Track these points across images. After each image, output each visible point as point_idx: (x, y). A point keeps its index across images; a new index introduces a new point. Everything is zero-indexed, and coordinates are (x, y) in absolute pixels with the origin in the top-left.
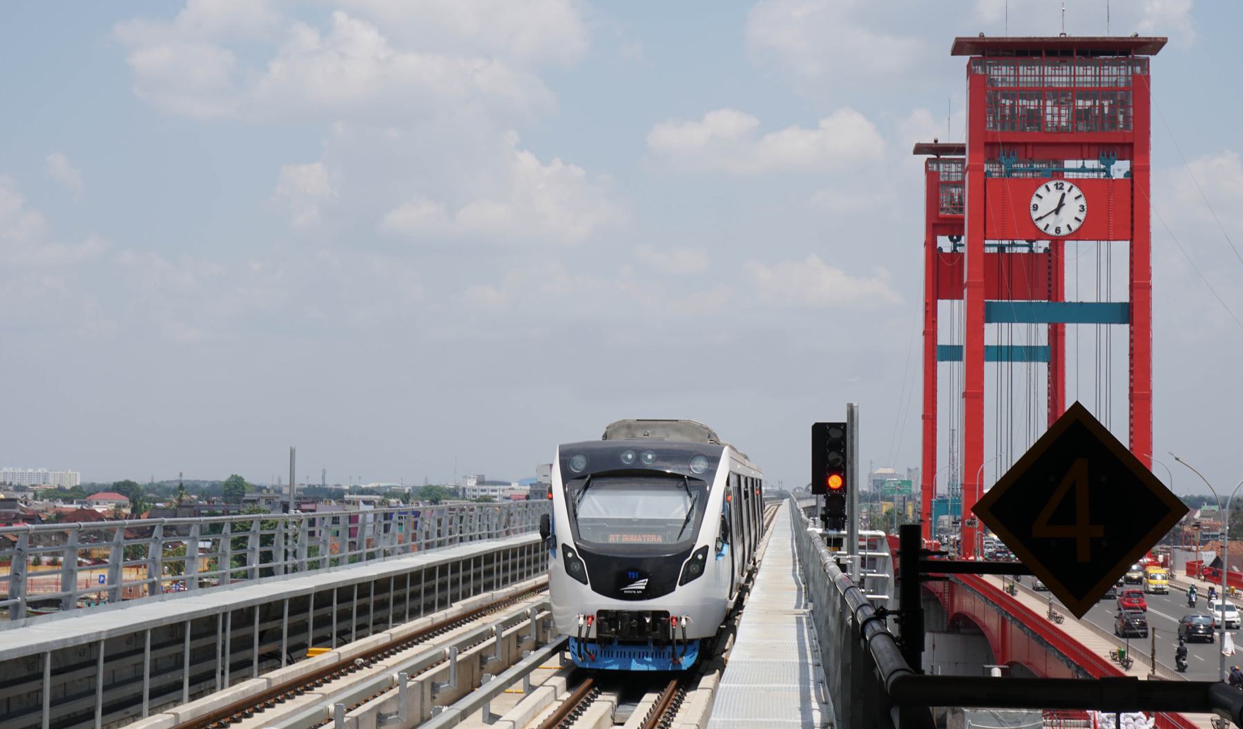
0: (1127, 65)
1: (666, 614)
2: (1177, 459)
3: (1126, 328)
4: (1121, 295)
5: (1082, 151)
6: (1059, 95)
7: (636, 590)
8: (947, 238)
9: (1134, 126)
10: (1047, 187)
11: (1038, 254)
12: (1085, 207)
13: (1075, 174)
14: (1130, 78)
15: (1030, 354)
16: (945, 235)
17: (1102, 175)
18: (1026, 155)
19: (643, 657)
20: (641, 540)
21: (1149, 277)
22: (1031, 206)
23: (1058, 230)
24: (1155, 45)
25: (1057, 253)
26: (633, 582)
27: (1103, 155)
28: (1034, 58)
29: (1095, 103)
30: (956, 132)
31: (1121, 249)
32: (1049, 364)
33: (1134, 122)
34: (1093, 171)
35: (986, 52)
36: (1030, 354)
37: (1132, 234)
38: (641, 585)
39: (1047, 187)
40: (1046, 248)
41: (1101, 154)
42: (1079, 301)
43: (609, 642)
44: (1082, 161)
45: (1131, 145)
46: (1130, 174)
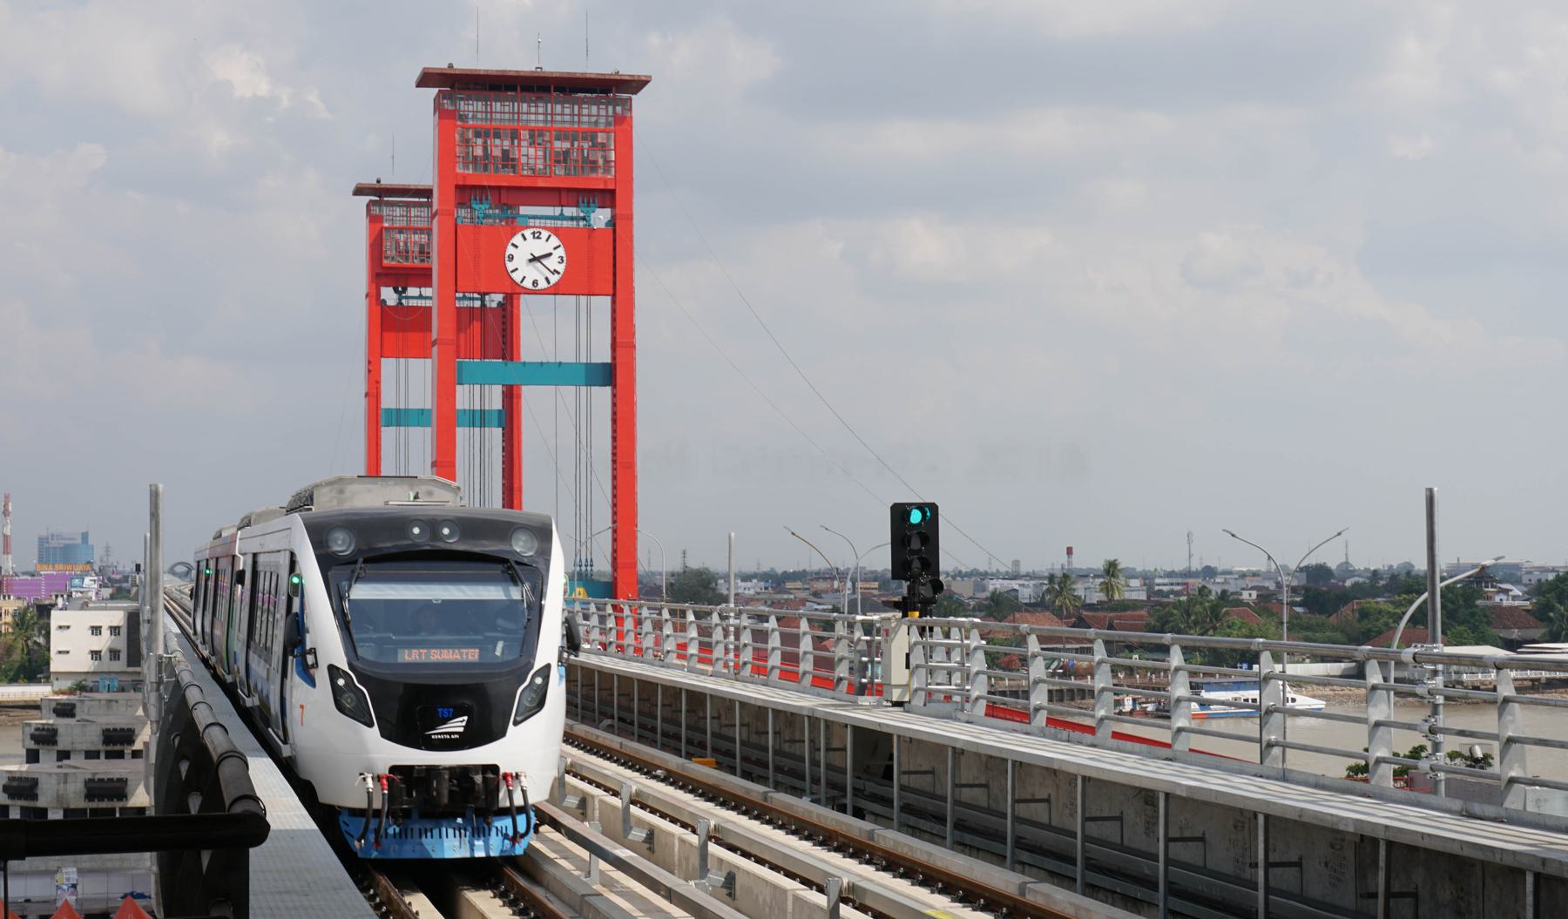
0: (607, 104)
1: (494, 769)
2: (793, 534)
3: (607, 391)
4: (603, 355)
5: (560, 195)
7: (450, 734)
8: (391, 289)
9: (615, 171)
10: (523, 235)
11: (491, 308)
12: (565, 259)
13: (553, 222)
14: (611, 119)
16: (389, 286)
17: (582, 224)
18: (500, 202)
19: (420, 836)
20: (458, 657)
21: (633, 334)
22: (506, 256)
23: (535, 283)
24: (636, 85)
25: (512, 307)
26: (445, 721)
27: (583, 202)
28: (509, 93)
29: (572, 145)
30: (420, 169)
31: (602, 304)
32: (503, 429)
33: (615, 167)
34: (572, 219)
35: (456, 86)
37: (615, 288)
38: (457, 725)
39: (523, 235)
40: (500, 302)
41: (580, 201)
42: (558, 361)
43: (407, 814)
44: (560, 208)
45: (613, 192)
46: (612, 223)
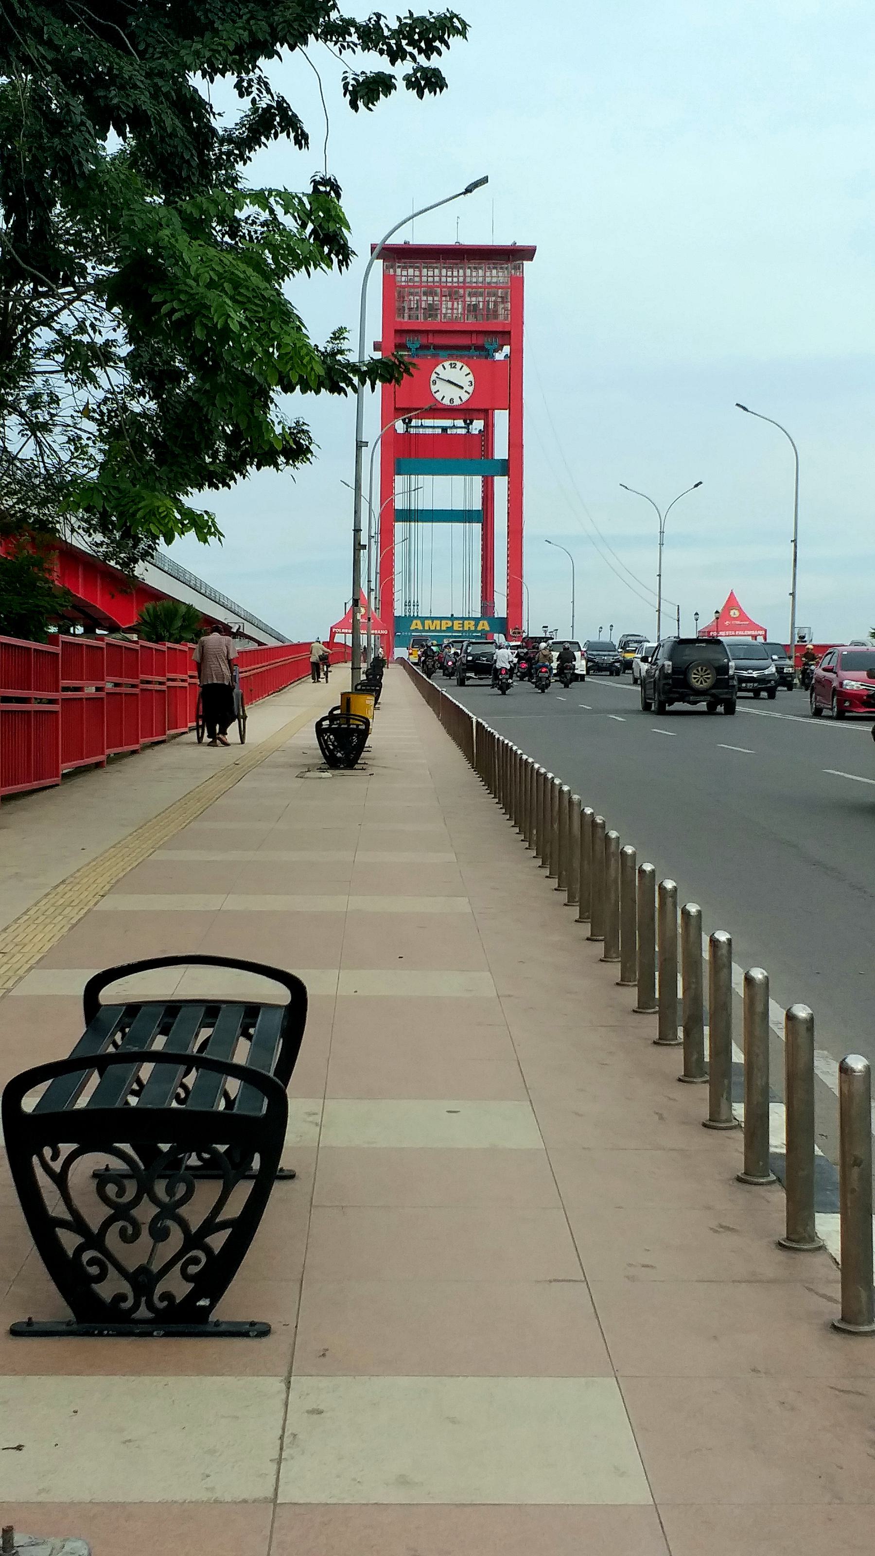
6: (452, 294)
15: (465, 516)
23: (452, 400)
24: (528, 253)
36: (465, 516)
45: (509, 333)
